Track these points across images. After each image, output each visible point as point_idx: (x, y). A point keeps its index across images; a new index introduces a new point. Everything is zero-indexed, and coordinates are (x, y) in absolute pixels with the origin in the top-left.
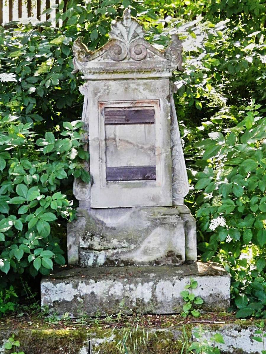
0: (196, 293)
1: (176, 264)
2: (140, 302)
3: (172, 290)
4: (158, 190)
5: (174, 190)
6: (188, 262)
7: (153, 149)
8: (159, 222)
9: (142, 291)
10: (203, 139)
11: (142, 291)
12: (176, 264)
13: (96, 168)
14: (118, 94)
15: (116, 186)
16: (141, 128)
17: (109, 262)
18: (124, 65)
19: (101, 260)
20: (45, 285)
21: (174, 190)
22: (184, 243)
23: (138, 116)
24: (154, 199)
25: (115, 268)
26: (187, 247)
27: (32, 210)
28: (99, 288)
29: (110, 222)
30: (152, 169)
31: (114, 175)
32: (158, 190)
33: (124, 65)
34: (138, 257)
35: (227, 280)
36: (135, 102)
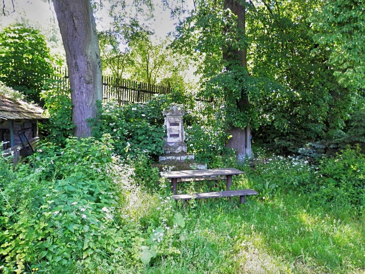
0: (188, 158)
1: (183, 153)
2: (178, 160)
3: (184, 158)
4: (180, 138)
5: (182, 139)
6: (185, 153)
7: (179, 131)
8: (180, 145)
9: (179, 158)
10: (305, 211)
11: (179, 158)
12: (183, 153)
13: (168, 134)
14: (172, 120)
15: (172, 138)
16: (176, 127)
17: (171, 153)
18: (174, 114)
19: (169, 152)
20: (160, 157)
21: (182, 139)
22: (185, 149)
23: (176, 124)
24: (179, 140)
25: (172, 154)
26: (21, 108)
27: (159, 142)
28: (170, 158)
29: (170, 145)
30: (179, 135)
31: (171, 136)
32: (180, 138)
33: (174, 114)
34: (176, 152)
35: (194, 156)
36: (176, 121)
